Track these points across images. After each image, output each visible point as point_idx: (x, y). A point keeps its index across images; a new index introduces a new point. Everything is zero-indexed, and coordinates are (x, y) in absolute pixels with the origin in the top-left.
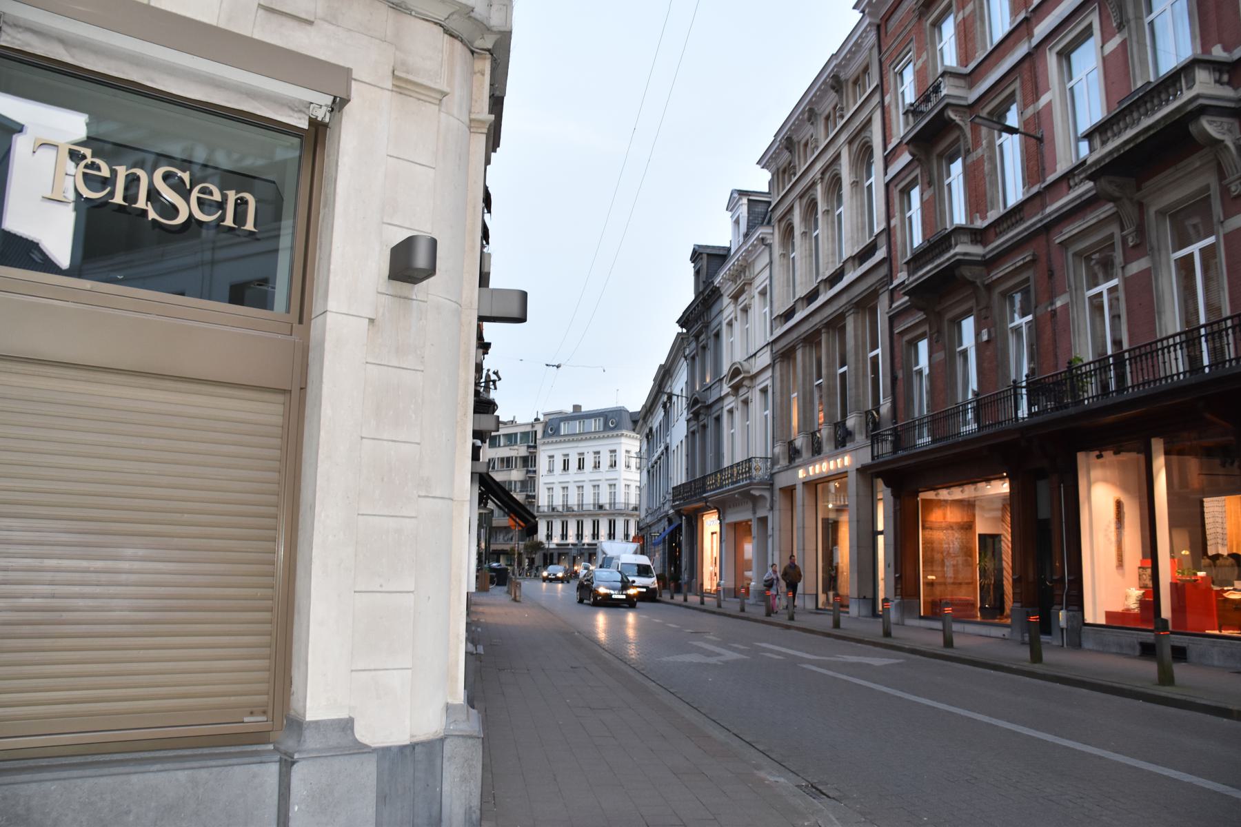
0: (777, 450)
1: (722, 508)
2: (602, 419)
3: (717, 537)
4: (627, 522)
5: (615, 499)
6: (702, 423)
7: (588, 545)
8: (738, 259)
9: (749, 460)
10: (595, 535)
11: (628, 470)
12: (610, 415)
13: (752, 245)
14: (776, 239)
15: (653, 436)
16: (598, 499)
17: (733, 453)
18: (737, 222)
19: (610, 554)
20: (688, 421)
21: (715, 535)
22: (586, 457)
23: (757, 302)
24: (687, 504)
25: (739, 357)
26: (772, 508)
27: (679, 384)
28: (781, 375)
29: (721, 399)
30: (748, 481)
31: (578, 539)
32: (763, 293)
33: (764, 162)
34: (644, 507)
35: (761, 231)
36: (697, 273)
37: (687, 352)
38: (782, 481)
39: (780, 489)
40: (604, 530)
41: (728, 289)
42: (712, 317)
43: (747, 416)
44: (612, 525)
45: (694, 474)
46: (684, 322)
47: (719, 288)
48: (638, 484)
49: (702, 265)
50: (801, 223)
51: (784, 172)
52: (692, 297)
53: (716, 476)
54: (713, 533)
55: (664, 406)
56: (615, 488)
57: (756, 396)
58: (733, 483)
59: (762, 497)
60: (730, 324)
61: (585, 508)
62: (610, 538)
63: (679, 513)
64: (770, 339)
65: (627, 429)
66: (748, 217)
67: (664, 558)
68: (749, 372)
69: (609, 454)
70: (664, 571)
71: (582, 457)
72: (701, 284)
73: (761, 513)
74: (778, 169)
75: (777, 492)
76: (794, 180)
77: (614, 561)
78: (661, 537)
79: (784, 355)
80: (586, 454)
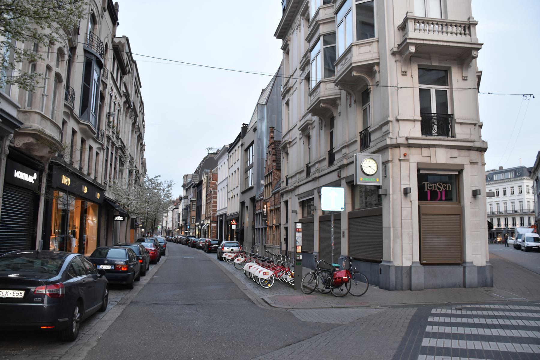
31: (506, 226)
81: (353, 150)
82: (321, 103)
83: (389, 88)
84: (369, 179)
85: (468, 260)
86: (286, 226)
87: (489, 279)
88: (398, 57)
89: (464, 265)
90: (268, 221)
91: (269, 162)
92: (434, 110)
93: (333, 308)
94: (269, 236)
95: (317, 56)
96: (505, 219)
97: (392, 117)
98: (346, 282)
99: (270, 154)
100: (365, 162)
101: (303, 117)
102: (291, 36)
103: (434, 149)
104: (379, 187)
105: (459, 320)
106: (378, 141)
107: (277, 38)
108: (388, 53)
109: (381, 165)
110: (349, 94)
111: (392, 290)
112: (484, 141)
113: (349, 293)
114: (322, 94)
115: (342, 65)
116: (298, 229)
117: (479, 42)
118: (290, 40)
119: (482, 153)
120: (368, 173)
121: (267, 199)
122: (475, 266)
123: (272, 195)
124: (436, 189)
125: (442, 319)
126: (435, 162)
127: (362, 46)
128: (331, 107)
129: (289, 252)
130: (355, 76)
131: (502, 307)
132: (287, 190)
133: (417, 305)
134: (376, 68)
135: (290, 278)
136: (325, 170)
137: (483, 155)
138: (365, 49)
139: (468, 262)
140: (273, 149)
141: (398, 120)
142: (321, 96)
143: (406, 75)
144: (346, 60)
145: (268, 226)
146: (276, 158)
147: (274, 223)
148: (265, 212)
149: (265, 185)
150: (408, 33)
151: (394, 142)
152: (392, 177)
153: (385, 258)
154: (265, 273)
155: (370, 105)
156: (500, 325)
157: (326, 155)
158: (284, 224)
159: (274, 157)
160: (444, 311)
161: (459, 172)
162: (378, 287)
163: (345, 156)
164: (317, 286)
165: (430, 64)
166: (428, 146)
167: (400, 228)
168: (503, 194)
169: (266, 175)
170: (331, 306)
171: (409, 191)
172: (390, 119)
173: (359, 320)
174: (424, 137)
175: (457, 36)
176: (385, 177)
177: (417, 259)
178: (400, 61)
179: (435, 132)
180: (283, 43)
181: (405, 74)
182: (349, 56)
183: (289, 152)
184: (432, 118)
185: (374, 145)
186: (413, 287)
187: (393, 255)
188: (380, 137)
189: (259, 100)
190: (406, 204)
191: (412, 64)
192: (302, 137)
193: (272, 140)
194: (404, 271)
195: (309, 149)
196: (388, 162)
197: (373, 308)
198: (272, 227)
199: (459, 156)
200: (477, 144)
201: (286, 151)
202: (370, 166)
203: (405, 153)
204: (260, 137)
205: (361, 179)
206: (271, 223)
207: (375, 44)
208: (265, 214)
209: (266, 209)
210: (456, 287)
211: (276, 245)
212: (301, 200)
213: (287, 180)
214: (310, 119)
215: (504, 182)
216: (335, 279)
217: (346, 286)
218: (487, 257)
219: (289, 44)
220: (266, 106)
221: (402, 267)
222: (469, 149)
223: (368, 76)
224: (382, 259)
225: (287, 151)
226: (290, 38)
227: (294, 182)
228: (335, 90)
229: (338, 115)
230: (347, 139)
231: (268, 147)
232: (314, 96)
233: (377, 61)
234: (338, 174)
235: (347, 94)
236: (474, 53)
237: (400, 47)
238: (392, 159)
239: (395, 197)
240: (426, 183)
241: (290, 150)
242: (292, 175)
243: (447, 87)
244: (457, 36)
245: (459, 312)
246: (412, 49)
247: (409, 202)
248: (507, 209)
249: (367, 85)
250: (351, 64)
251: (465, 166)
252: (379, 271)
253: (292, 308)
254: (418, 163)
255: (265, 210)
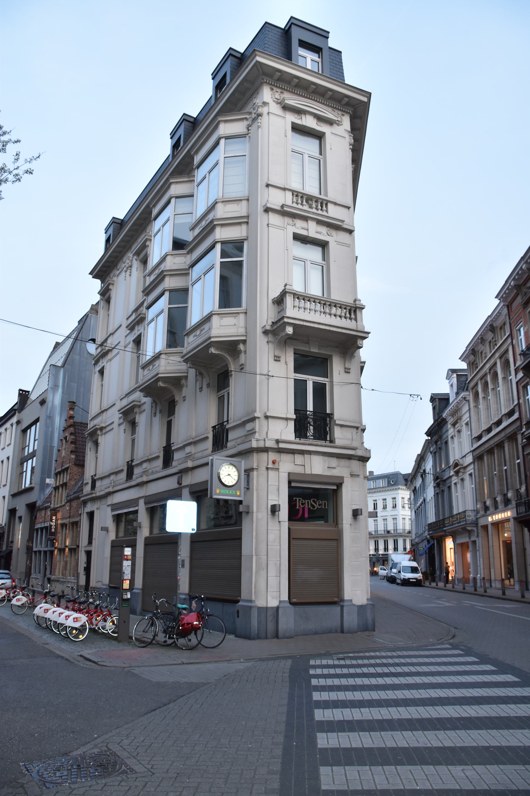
0: (478, 506)
1: (454, 536)
2: (386, 479)
3: (452, 551)
4: (405, 541)
5: (396, 527)
6: (441, 489)
7: (382, 555)
8: (453, 406)
9: (465, 512)
10: (386, 549)
11: (404, 509)
12: (391, 477)
13: (460, 400)
14: (471, 398)
15: (416, 492)
16: (387, 527)
17: (458, 507)
18: (452, 385)
19: (396, 561)
20: (434, 487)
21: (452, 550)
22: (378, 502)
23: (464, 428)
24: (436, 533)
25: (458, 456)
26: (478, 536)
27: (429, 465)
28: (478, 468)
29: (450, 477)
30: (465, 523)
31: (376, 551)
32: (467, 424)
33: (463, 358)
34: (414, 532)
35: (462, 394)
36: (434, 408)
37: (432, 449)
38: (482, 522)
39: (481, 526)
40: (391, 546)
41: (451, 420)
42: (443, 433)
43: (463, 487)
44: (396, 542)
45: (439, 517)
46: (429, 434)
47: (445, 419)
48: (410, 517)
49: (436, 405)
50: (482, 392)
51: (473, 363)
52: (432, 422)
53: (449, 519)
54: (451, 549)
55: (422, 476)
56: (396, 521)
57: (467, 477)
58: (458, 523)
59: (472, 530)
60: (452, 437)
61: (379, 533)
62: (395, 551)
63: (432, 537)
64: (472, 449)
65: (402, 485)
66: (457, 384)
67: (426, 562)
68: (463, 465)
69: (391, 500)
70: (427, 570)
71: (375, 502)
72: (436, 415)
73: (473, 539)
74: (470, 362)
75: (480, 528)
76: (477, 370)
77: (398, 565)
78: (424, 550)
79: (479, 458)
80: (378, 500)
81: (202, 449)
82: (159, 381)
83: (258, 376)
84: (227, 492)
85: (347, 597)
86: (88, 549)
87: (370, 622)
88: (271, 337)
89: (342, 604)
90: (57, 541)
91: (63, 453)
92: (310, 407)
93: (184, 664)
94: (58, 563)
95: (157, 316)
96: (375, 542)
97: (260, 412)
98: (195, 629)
99: (66, 441)
100: (223, 468)
101: (127, 395)
102: (115, 279)
103: (310, 455)
104: (241, 502)
105: (345, 671)
106: (239, 441)
107: (93, 277)
108: (259, 331)
109: (243, 473)
110: (200, 374)
111: (253, 639)
112: (366, 449)
113: (200, 645)
114: (162, 369)
115: (195, 336)
116: (127, 556)
117: (366, 330)
118: (113, 284)
119: (364, 464)
120: (226, 483)
121: (57, 508)
122: (355, 605)
123: (66, 503)
124: (310, 506)
125: (326, 671)
126: (310, 473)
127: (225, 317)
128: (172, 388)
129: (92, 588)
130: (214, 354)
131: (389, 654)
132: (93, 497)
133: (289, 656)
134: (241, 347)
135: (111, 626)
136: (157, 472)
137: (365, 466)
138: (228, 321)
139: (346, 600)
140: (71, 434)
141: (267, 417)
142: (160, 372)
143: (279, 361)
144: (202, 331)
145: (56, 548)
146: (76, 448)
147: (67, 544)
148: (53, 527)
149: (54, 486)
150: (286, 311)
151: (261, 444)
152: (256, 490)
153: (244, 595)
154: (77, 618)
155: (230, 391)
156: (392, 673)
157: (160, 452)
158: (85, 547)
159: (72, 446)
160: (324, 662)
161: (337, 486)
162: (234, 636)
163: (189, 456)
164: (155, 635)
165: (309, 350)
166: (302, 452)
167: (266, 557)
168: (373, 508)
169: (57, 471)
170: (181, 662)
171: (277, 509)
172: (256, 415)
173: (225, 678)
174: (298, 440)
175: (341, 319)
176: (248, 489)
177: (285, 597)
178: (273, 343)
179: (311, 434)
180: (102, 288)
181: (278, 359)
182: (206, 327)
183: (99, 441)
184: (308, 417)
185: (232, 446)
186: (280, 634)
187: (255, 593)
188: (242, 437)
189: (49, 357)
190: (273, 526)
191: (287, 348)
192: (123, 422)
193: (71, 421)
194: (270, 613)
195: (133, 441)
196: (252, 469)
197: (236, 663)
198: (64, 550)
199: (338, 466)
200: (360, 453)
201: (94, 439)
202: (229, 475)
203: (274, 459)
204: (50, 413)
205: (218, 492)
206: (61, 544)
207: (242, 317)
208: (53, 530)
209: (55, 523)
210: (333, 633)
211: (69, 578)
212: (117, 513)
213: (94, 482)
214: (138, 400)
215: (375, 492)
216: (183, 625)
217: (196, 634)
218: (368, 593)
219: (111, 290)
220: (62, 369)
221: (267, 608)
222: (350, 457)
223: (229, 355)
224: (240, 596)
225: (97, 439)
226: (114, 281)
227: (107, 486)
228: (180, 365)
229: (182, 399)
230: (194, 434)
231: (63, 431)
232: (149, 370)
233: (244, 338)
234: (178, 479)
235: (198, 374)
236: (359, 342)
237: (274, 326)
238: (257, 466)
239: (260, 516)
240: (298, 499)
241: (101, 440)
242: (104, 475)
243: (326, 379)
244: (341, 319)
245: (342, 662)
246: (290, 330)
247: (277, 523)
248: (377, 528)
249: (227, 366)
250: (210, 338)
251: (345, 479)
252: (236, 614)
253: (130, 667)
254: (289, 473)
255: (53, 524)
